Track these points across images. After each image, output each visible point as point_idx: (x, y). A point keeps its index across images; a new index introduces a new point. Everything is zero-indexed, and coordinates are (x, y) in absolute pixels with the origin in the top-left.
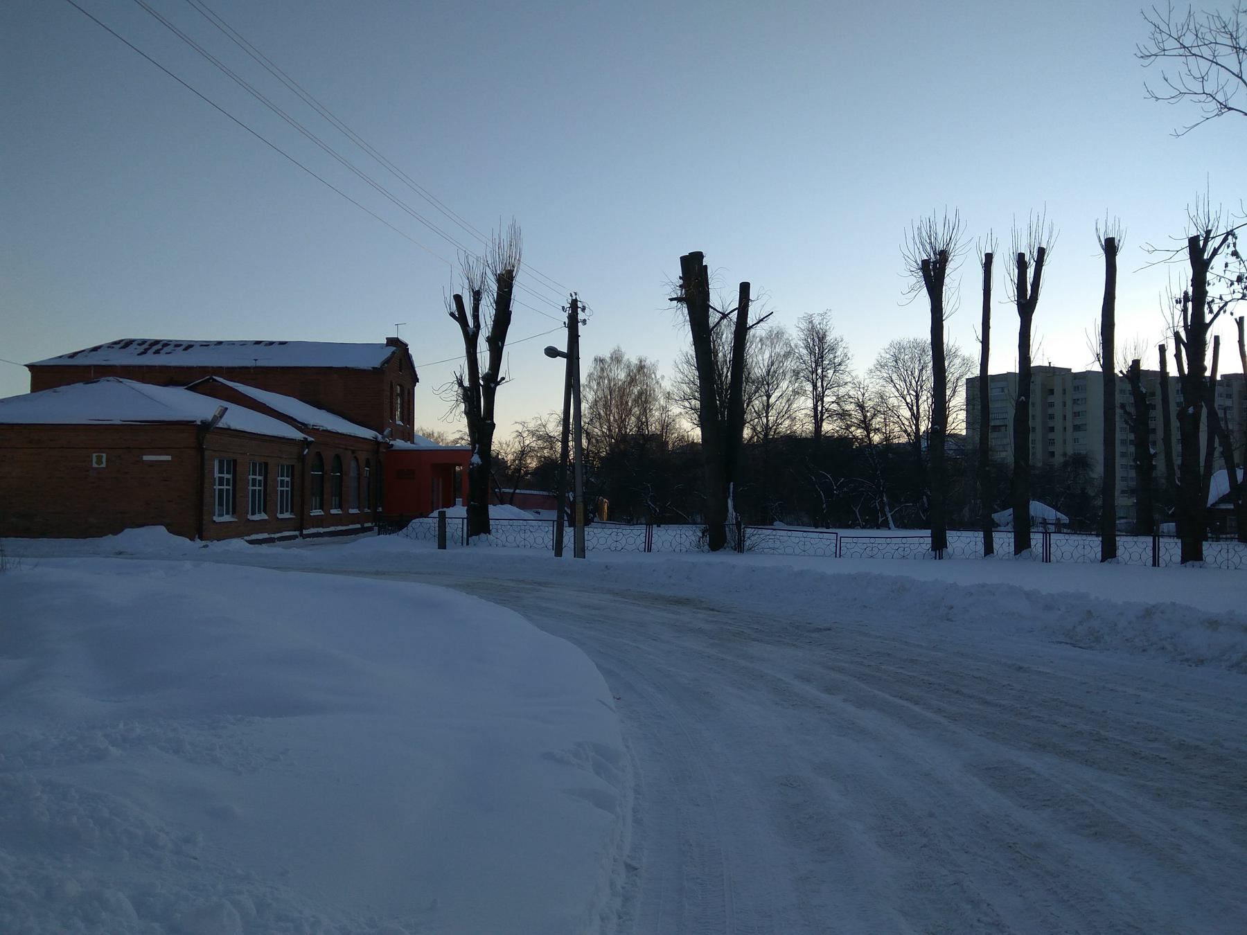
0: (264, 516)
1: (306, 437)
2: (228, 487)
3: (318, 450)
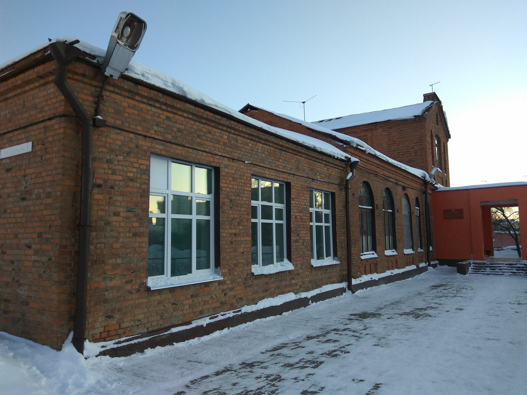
0: (287, 266)
1: (349, 156)
3: (366, 180)
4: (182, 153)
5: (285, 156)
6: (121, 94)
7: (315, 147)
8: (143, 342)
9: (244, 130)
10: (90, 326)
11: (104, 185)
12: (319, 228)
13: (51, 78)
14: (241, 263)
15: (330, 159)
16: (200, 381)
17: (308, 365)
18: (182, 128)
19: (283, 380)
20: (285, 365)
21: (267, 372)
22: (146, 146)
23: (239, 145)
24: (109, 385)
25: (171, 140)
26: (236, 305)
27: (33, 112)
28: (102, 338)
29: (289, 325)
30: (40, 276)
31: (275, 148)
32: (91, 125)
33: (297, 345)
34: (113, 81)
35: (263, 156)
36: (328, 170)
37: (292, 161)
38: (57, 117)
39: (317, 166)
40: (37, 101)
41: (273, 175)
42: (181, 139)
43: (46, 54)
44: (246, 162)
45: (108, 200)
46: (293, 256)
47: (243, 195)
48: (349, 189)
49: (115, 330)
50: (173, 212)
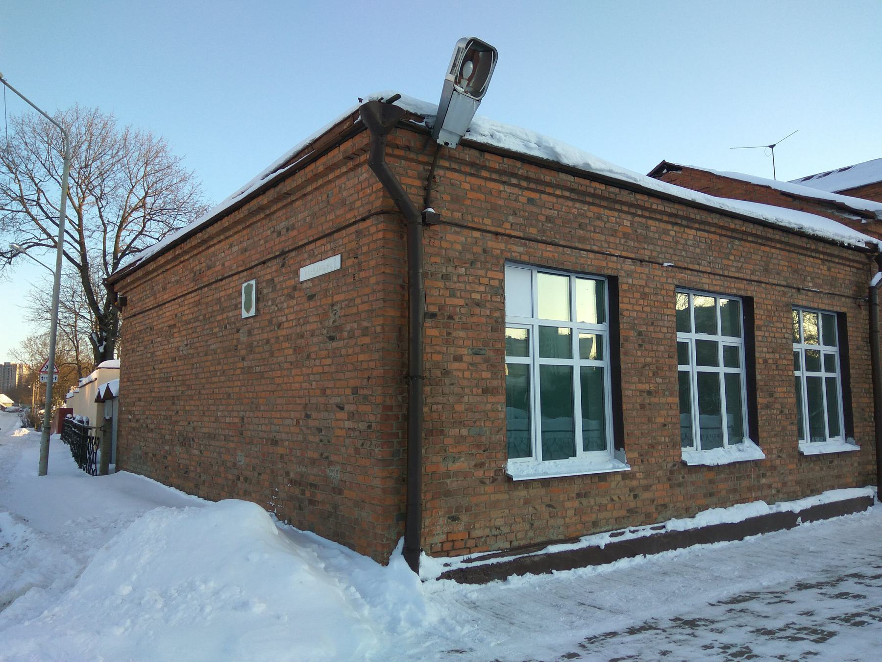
0: (750, 451)
1: (875, 241)
2: (830, 375)
4: (554, 256)
5: (741, 248)
6: (460, 170)
7: (801, 228)
8: (505, 563)
9: (661, 208)
10: (427, 530)
11: (439, 313)
12: (813, 383)
13: (363, 158)
14: (662, 443)
15: (834, 248)
16: (602, 640)
17: (805, 636)
18: (553, 215)
19: (757, 656)
20: (758, 630)
21: (724, 639)
22: (498, 249)
23: (651, 235)
24: (458, 628)
25: (536, 237)
26: (655, 516)
27: (340, 212)
28: (444, 551)
29: (760, 559)
30: (357, 452)
31: (721, 235)
32: (419, 223)
33: (778, 597)
34: (449, 151)
35: (698, 251)
36: (829, 269)
37: (754, 257)
38: (373, 215)
39: (805, 264)
40: (345, 194)
41: (717, 285)
42: (552, 233)
43: (355, 122)
44: (666, 264)
45: (446, 337)
46: (762, 434)
47: (661, 323)
48: (876, 304)
49: (462, 540)
50: (542, 355)
